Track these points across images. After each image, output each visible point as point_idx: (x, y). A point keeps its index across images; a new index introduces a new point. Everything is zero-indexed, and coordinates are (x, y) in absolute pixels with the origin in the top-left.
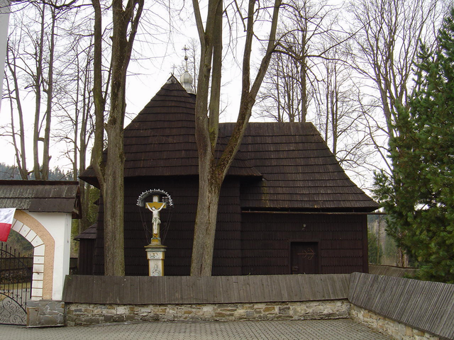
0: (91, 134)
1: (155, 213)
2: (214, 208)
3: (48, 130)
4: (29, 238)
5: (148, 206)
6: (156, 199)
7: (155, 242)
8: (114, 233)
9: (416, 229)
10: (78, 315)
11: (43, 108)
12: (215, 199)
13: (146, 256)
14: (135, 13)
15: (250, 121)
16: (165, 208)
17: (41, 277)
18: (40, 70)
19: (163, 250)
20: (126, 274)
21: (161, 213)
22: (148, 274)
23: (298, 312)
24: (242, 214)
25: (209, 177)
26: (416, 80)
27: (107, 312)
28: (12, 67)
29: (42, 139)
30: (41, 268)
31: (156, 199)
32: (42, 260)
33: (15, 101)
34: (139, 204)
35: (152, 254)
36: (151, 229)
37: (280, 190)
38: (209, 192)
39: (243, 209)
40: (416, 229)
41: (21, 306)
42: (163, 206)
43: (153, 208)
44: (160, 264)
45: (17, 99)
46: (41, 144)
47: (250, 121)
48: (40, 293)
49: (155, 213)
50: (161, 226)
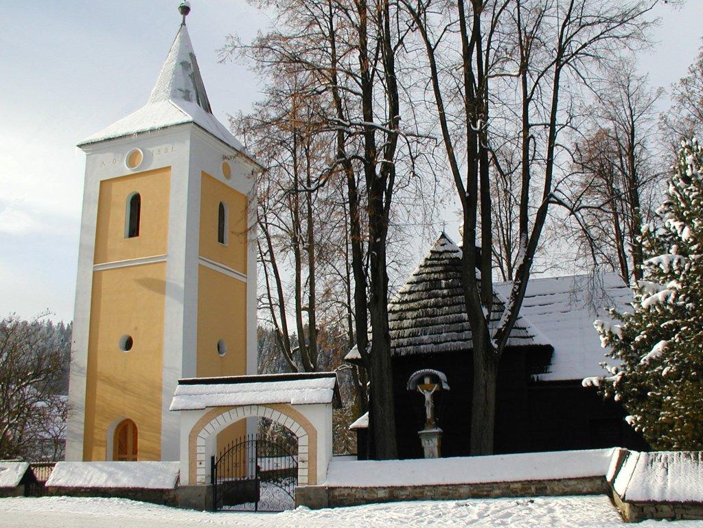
0: (565, 56)
1: (428, 396)
2: (492, 387)
3: (312, 298)
4: (293, 430)
10: (342, 500)
11: (305, 274)
12: (492, 377)
14: (388, 183)
17: (306, 465)
18: (297, 224)
21: (434, 396)
23: (555, 491)
25: (484, 353)
26: (631, 250)
27: (369, 496)
28: (264, 225)
29: (305, 309)
30: (306, 457)
31: (427, 381)
32: (306, 450)
33: (270, 265)
34: (410, 387)
36: (425, 414)
38: (485, 370)
41: (289, 494)
45: (273, 261)
46: (305, 314)
48: (306, 480)
49: (428, 396)
50: (435, 410)
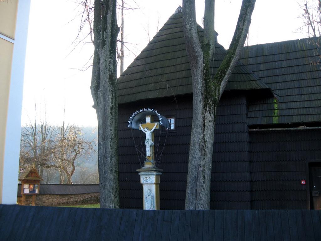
2: (210, 125)
5: (141, 127)
6: (148, 120)
7: (148, 165)
8: (196, 180)
9: (219, 77)
13: (140, 181)
15: (246, 45)
16: (158, 128)
19: (155, 173)
20: (120, 207)
21: (155, 134)
22: (183, 208)
24: (250, 133)
31: (148, 120)
35: (145, 179)
37: (294, 105)
39: (250, 127)
40: (219, 77)
42: (155, 126)
43: (146, 129)
44: (154, 188)
47: (246, 45)
